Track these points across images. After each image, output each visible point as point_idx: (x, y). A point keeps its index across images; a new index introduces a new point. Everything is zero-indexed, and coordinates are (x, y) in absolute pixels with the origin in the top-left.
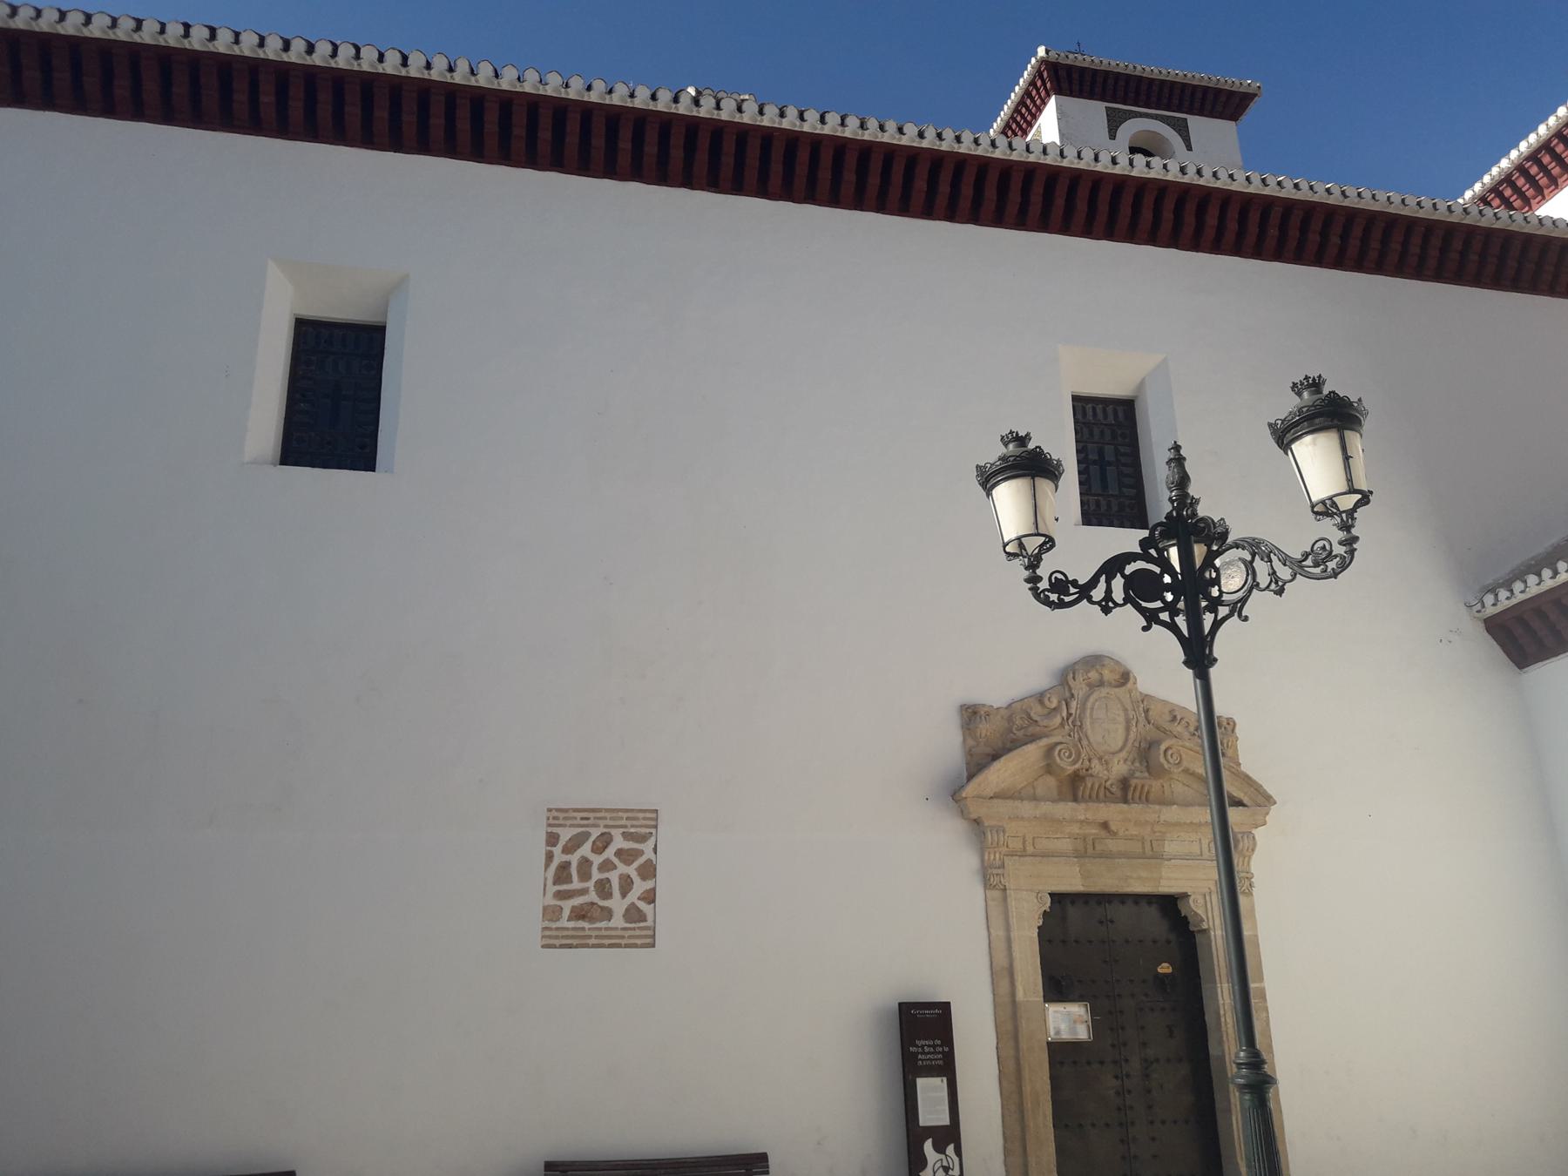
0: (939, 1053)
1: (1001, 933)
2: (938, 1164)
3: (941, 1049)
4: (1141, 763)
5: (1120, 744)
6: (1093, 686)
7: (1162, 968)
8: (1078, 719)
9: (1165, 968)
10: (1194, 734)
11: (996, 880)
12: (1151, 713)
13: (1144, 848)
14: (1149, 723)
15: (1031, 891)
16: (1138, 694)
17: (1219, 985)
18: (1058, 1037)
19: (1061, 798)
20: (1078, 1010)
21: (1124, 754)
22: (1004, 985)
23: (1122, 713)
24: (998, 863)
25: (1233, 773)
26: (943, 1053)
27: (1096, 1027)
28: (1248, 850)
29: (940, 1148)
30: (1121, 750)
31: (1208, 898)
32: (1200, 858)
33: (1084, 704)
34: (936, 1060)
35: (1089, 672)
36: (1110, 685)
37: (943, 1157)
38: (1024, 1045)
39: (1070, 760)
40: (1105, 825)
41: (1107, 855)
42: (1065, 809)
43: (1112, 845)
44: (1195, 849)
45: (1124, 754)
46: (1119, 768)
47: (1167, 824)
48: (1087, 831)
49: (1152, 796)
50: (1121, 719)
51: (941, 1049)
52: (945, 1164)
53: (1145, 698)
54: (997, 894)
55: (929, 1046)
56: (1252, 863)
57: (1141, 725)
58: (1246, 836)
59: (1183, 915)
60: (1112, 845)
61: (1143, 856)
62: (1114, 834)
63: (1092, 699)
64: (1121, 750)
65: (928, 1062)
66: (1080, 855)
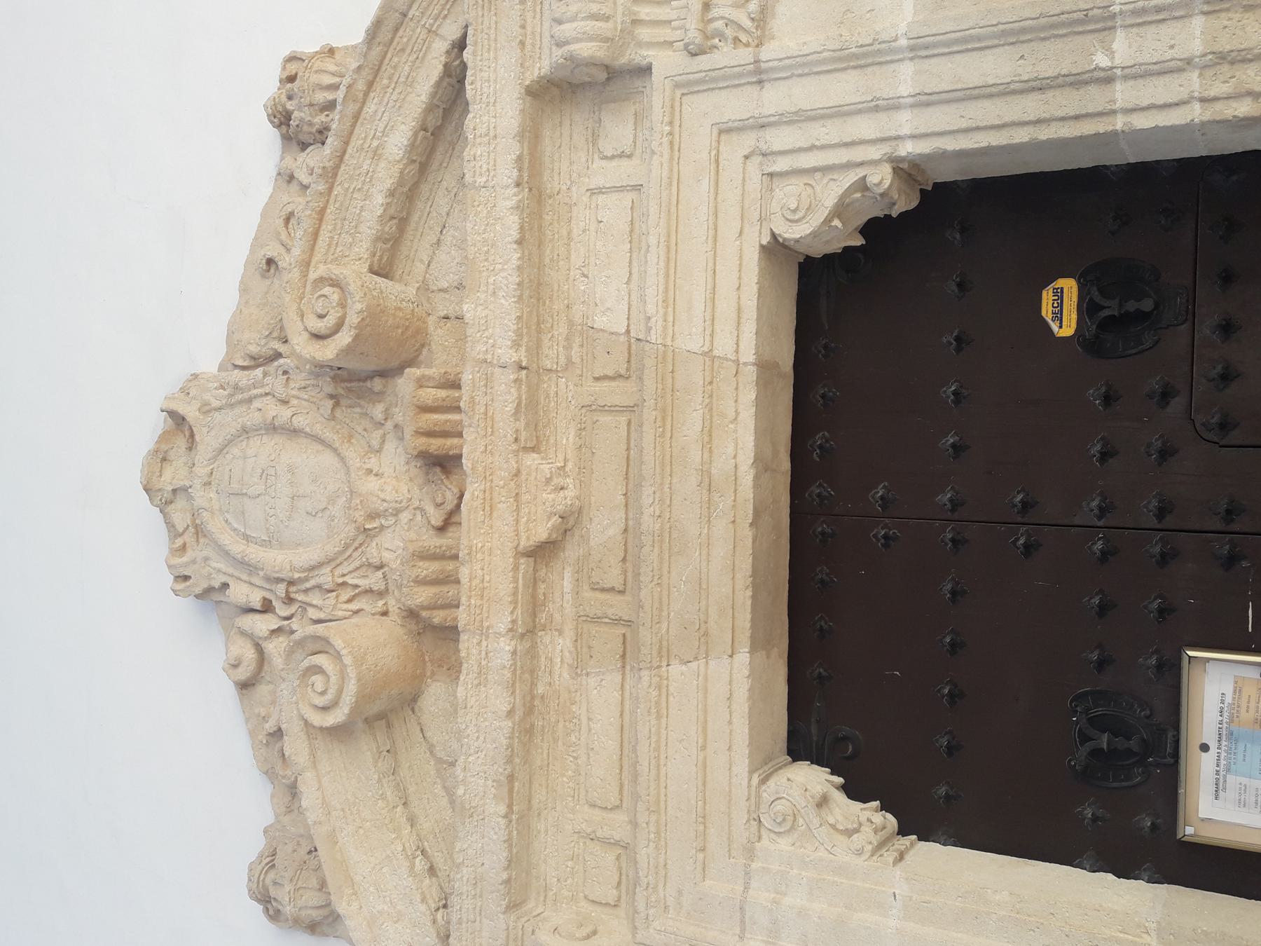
5: (328, 459)
7: (1058, 317)
14: (278, 355)
15: (750, 853)
17: (1119, 123)
21: (351, 453)
25: (370, 85)
28: (607, 18)
30: (342, 459)
31: (782, 164)
33: (244, 564)
44: (615, 210)
48: (569, 609)
59: (859, 241)
63: (226, 539)
64: (342, 459)
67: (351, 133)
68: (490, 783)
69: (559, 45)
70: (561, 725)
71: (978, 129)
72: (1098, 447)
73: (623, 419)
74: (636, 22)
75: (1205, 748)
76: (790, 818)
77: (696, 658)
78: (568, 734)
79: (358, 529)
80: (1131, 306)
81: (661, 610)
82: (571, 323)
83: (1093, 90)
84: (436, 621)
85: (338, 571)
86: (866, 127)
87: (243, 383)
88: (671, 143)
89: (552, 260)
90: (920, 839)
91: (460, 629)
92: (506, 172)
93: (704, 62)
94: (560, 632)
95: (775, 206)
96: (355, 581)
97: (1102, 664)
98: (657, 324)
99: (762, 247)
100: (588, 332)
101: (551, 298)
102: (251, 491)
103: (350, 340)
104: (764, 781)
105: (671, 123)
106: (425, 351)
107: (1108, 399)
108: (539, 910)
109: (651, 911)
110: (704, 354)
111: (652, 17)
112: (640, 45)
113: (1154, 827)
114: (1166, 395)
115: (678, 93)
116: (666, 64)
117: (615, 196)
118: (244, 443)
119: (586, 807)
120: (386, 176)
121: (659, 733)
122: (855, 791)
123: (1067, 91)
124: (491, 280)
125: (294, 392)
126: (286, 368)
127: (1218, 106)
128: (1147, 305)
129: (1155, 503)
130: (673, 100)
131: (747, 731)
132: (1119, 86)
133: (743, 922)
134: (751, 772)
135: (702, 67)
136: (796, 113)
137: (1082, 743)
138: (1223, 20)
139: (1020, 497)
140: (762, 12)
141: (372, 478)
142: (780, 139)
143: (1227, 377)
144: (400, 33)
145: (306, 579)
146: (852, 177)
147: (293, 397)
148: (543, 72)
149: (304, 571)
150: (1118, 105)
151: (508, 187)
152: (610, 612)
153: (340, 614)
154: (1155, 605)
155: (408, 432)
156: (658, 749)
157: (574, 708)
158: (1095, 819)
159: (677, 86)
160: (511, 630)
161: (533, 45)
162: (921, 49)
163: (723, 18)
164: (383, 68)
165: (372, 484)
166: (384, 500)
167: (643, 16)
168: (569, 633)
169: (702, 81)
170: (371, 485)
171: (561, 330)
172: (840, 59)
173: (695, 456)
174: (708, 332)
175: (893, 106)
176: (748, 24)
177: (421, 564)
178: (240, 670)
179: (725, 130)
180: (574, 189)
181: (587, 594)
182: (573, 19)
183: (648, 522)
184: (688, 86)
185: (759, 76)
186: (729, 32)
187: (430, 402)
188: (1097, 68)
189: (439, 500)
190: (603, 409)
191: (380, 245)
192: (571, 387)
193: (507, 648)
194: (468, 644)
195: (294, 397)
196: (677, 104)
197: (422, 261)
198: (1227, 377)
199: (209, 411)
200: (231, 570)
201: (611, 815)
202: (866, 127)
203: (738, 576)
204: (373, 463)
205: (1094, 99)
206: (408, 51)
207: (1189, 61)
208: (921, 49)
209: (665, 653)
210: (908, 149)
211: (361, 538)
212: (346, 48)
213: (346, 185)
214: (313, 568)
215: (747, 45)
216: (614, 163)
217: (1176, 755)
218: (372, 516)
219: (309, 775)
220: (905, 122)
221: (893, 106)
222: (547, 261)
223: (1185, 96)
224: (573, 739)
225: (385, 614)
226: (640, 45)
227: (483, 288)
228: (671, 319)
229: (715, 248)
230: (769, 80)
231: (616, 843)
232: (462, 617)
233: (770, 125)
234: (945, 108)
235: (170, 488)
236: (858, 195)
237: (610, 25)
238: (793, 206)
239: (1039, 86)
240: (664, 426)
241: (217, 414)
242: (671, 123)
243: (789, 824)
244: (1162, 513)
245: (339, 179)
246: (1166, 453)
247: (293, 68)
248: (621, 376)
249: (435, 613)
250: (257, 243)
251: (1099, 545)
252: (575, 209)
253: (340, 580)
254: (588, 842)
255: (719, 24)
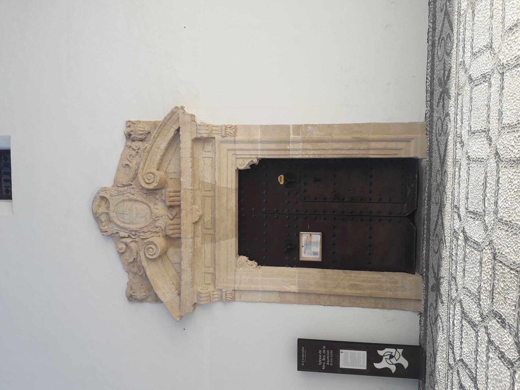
0: (326, 352)
1: (260, 295)
2: (388, 361)
3: (324, 351)
4: (157, 194)
5: (145, 206)
6: (110, 221)
7: (281, 181)
8: (132, 232)
9: (281, 180)
10: (137, 152)
11: (229, 296)
12: (125, 183)
13: (208, 197)
15: (235, 271)
16: (114, 188)
18: (319, 254)
19: (179, 246)
20: (304, 237)
21: (152, 205)
22: (288, 296)
23: (126, 203)
24: (219, 293)
25: (158, 136)
26: (326, 350)
27: (313, 229)
29: (379, 359)
30: (149, 206)
31: (238, 157)
32: (214, 158)
33: (124, 228)
34: (330, 354)
35: (101, 220)
36: (108, 208)
37: (384, 358)
38: (323, 290)
39: (155, 249)
40: (196, 223)
41: (214, 219)
42: (187, 241)
43: (208, 218)
44: (208, 161)
45: (152, 205)
46: (160, 209)
47: (193, 182)
49: (177, 189)
50: (129, 204)
51: (324, 351)
52: (388, 357)
53: (116, 184)
54: (237, 295)
55: (322, 358)
56: (217, 124)
57: (132, 191)
58: (198, 131)
60: (208, 218)
61: (213, 197)
62: (201, 217)
63: (119, 223)
64: (149, 206)
65: (331, 359)
66: (214, 240)
67: (153, 144)
68: (188, 265)
69: (199, 134)
70: (199, 254)
71: (270, 155)
72: (287, 202)
73: (211, 198)
74: (213, 130)
75: (303, 247)
76: (242, 264)
77: (226, 240)
78: (201, 255)
79: (153, 220)
80: (292, 180)
81: (219, 232)
82: (199, 181)
83: (287, 151)
84: (173, 237)
85: (148, 228)
86: (253, 153)
87: (122, 190)
88: (219, 151)
89: (196, 169)
90: (261, 266)
91: (181, 237)
92: (188, 154)
93: (225, 138)
94: (199, 237)
95: (238, 163)
96: (152, 230)
97: (288, 235)
98: (217, 182)
99: (235, 170)
100: (203, 183)
101: (196, 176)
102: (126, 213)
103: (157, 185)
104: (237, 259)
105: (219, 148)
106: (166, 185)
107: (288, 194)
108: (196, 287)
109: (218, 283)
110: (226, 187)
111: (215, 129)
112: (213, 134)
113: (296, 259)
114: (297, 194)
115: (220, 143)
116: (218, 137)
117: (208, 159)
118: (123, 203)
119: (204, 268)
120: (160, 153)
121: (219, 253)
122: (251, 259)
123: (284, 151)
124: (186, 174)
125: (136, 193)
126: (133, 187)
127: (304, 156)
128: (294, 180)
129: (295, 210)
130: (219, 144)
131: (235, 251)
132: (291, 151)
133: (235, 282)
134: (235, 258)
135: (225, 139)
136: (241, 149)
137: (286, 248)
138: (304, 144)
139: (276, 210)
140: (235, 131)
141: (156, 210)
142: (238, 152)
143: (305, 191)
144: (165, 127)
145: (140, 230)
146: (250, 160)
147: (136, 193)
148: (195, 137)
149: (140, 229)
150: (290, 154)
151: (189, 157)
152: (209, 233)
153: (149, 237)
154: (296, 226)
155: (167, 201)
156: (219, 256)
157: (202, 250)
158: (288, 259)
159: (220, 142)
160: (191, 237)
161: (193, 132)
162: (262, 142)
163: (228, 132)
164: (161, 132)
165: (156, 211)
166: (160, 214)
167: (214, 129)
168: (200, 237)
169: (225, 142)
170: (156, 211)
171: (198, 182)
172: (249, 142)
173: (225, 205)
174: (227, 184)
175: (257, 150)
176: (233, 133)
177: (170, 226)
178: (122, 250)
179: (228, 150)
180: (199, 157)
181: (204, 230)
182: (202, 130)
183: (217, 217)
184: (222, 142)
185: (235, 142)
186: (229, 134)
187: (171, 196)
188: (288, 148)
189: (172, 214)
190: (206, 196)
191: (158, 165)
192: (200, 192)
193: (191, 241)
194: (183, 241)
195: (136, 193)
196: (220, 144)
197: (165, 167)
198: (305, 191)
199: (112, 196)
200: (119, 229)
201: (210, 268)
202: (253, 153)
203: (233, 225)
204: (156, 207)
205: (287, 153)
206: (166, 130)
207: (300, 149)
208: (262, 142)
209: (220, 239)
210: (259, 157)
211: (154, 221)
212: (143, 121)
213: (152, 154)
214: (142, 228)
215: (233, 136)
216: (207, 153)
217: (299, 248)
218: (156, 217)
219: (148, 268)
220: (259, 153)
221: (257, 150)
222: (195, 170)
223: (299, 154)
224: (202, 256)
225: (159, 236)
226: (213, 134)
227: (184, 176)
228: (220, 181)
229: (227, 169)
230: (237, 143)
231: (211, 273)
232: (182, 236)
233: (236, 150)
234: (266, 151)
235: (101, 212)
236: (251, 162)
237: (209, 131)
238: (241, 164)
239: (280, 150)
240: (219, 200)
241: (114, 197)
242: (219, 148)
243: (241, 266)
244: (296, 212)
245: (150, 152)
246: (297, 203)
247: (129, 124)
248: (210, 191)
249: (173, 235)
250: (121, 160)
251: (287, 217)
252: (200, 160)
253: (148, 230)
254: (205, 274)
255: (228, 133)
